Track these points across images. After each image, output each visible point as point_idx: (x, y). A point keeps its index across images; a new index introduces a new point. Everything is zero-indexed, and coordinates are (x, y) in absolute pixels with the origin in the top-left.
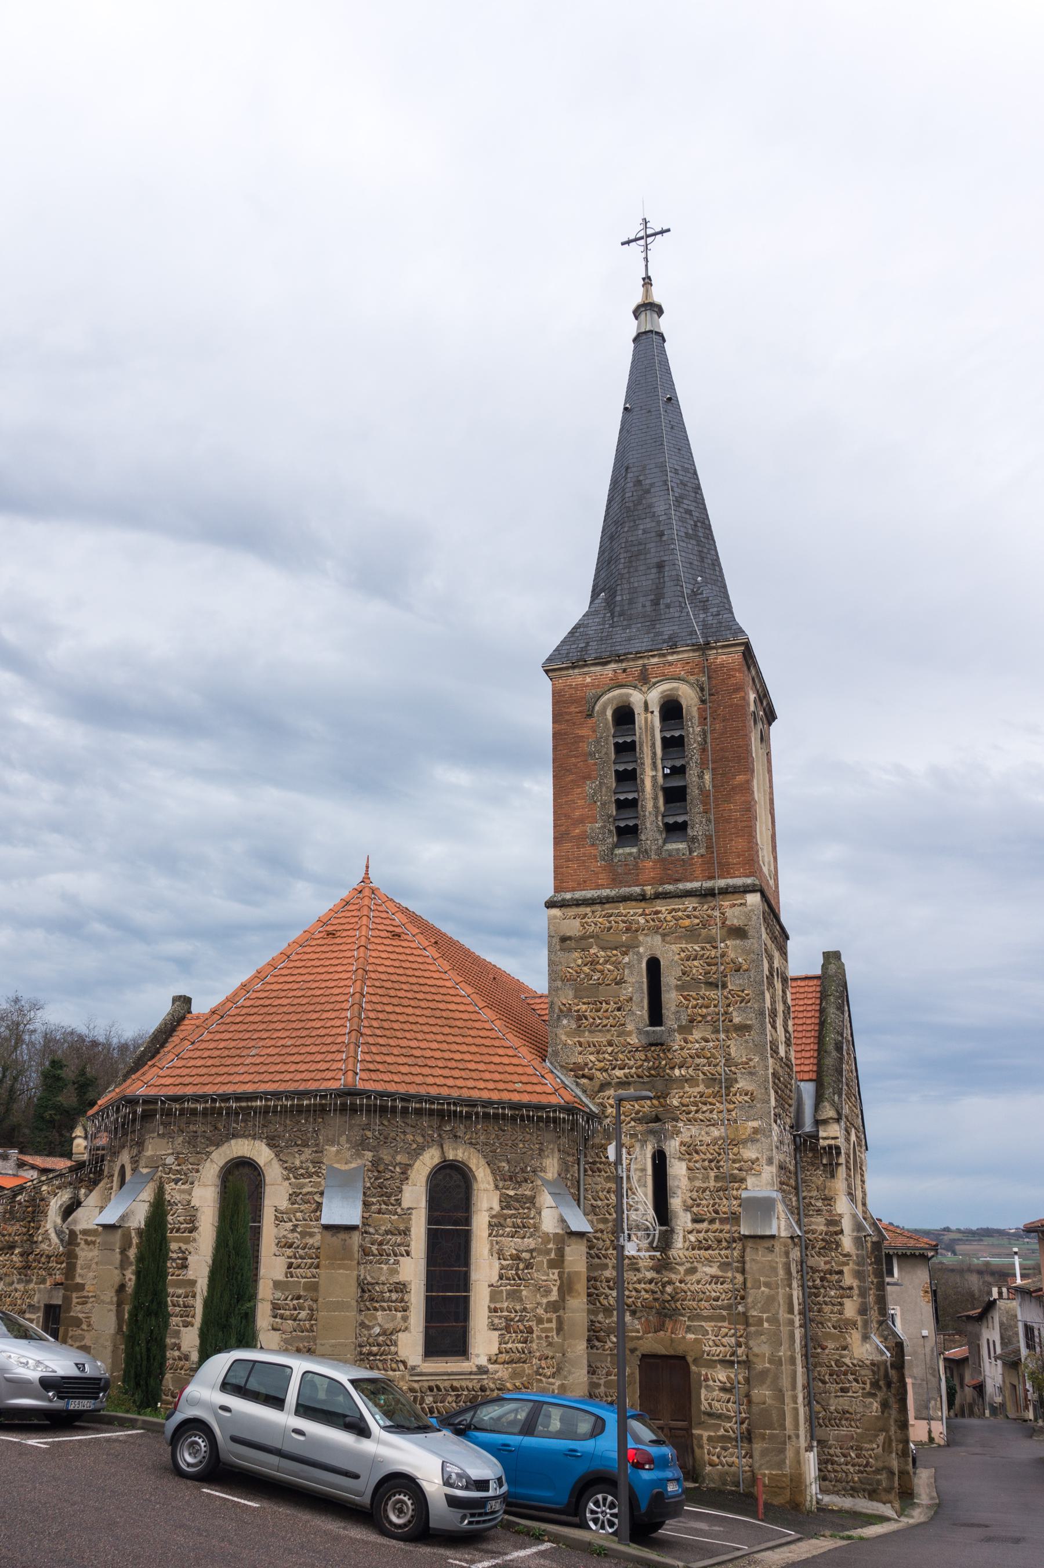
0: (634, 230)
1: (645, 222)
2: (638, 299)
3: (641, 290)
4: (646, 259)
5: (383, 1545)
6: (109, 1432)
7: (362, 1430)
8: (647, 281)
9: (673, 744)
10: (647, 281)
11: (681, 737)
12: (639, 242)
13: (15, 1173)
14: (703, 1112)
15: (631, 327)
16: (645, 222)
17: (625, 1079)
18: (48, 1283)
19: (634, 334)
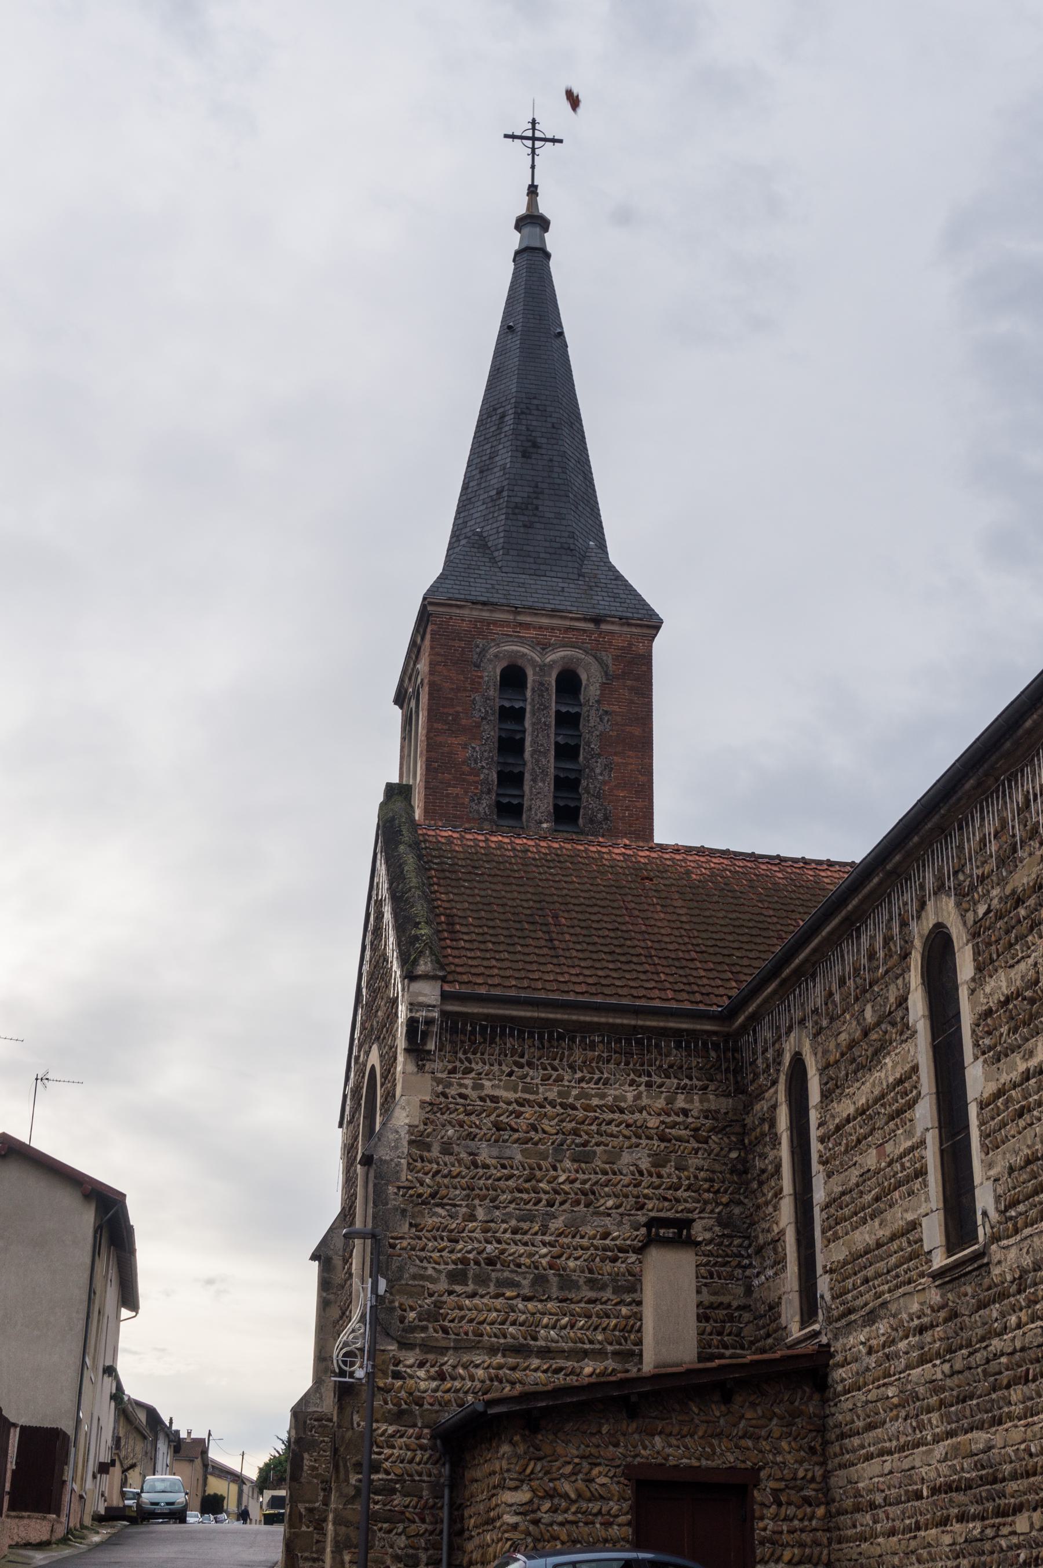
0: (522, 127)
1: (534, 122)
2: (522, 210)
3: (525, 199)
4: (533, 167)
5: (364, 1074)
6: (539, 1019)
7: (373, 1067)
8: (533, 191)
9: (567, 721)
10: (533, 191)
11: (578, 715)
12: (526, 142)
13: (990, 1454)
14: (482, 1297)
15: (514, 241)
16: (534, 122)
17: (521, 1340)
18: (445, 1117)
19: (516, 247)
